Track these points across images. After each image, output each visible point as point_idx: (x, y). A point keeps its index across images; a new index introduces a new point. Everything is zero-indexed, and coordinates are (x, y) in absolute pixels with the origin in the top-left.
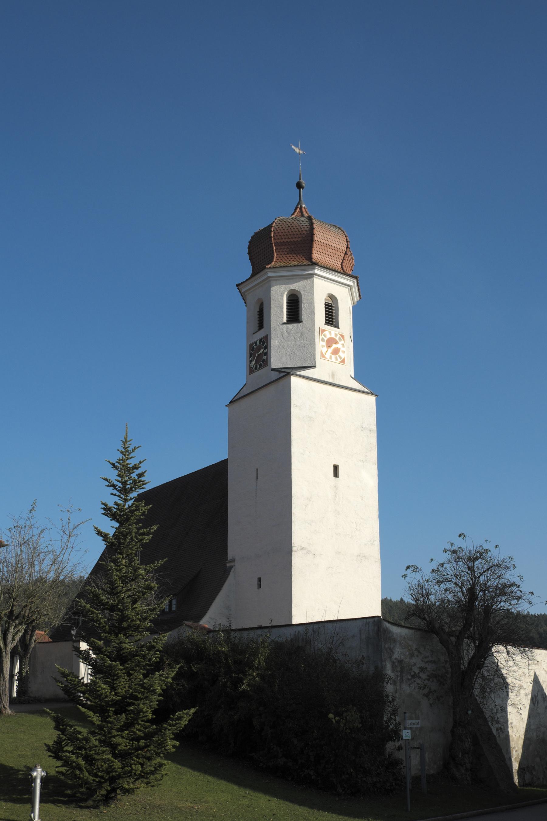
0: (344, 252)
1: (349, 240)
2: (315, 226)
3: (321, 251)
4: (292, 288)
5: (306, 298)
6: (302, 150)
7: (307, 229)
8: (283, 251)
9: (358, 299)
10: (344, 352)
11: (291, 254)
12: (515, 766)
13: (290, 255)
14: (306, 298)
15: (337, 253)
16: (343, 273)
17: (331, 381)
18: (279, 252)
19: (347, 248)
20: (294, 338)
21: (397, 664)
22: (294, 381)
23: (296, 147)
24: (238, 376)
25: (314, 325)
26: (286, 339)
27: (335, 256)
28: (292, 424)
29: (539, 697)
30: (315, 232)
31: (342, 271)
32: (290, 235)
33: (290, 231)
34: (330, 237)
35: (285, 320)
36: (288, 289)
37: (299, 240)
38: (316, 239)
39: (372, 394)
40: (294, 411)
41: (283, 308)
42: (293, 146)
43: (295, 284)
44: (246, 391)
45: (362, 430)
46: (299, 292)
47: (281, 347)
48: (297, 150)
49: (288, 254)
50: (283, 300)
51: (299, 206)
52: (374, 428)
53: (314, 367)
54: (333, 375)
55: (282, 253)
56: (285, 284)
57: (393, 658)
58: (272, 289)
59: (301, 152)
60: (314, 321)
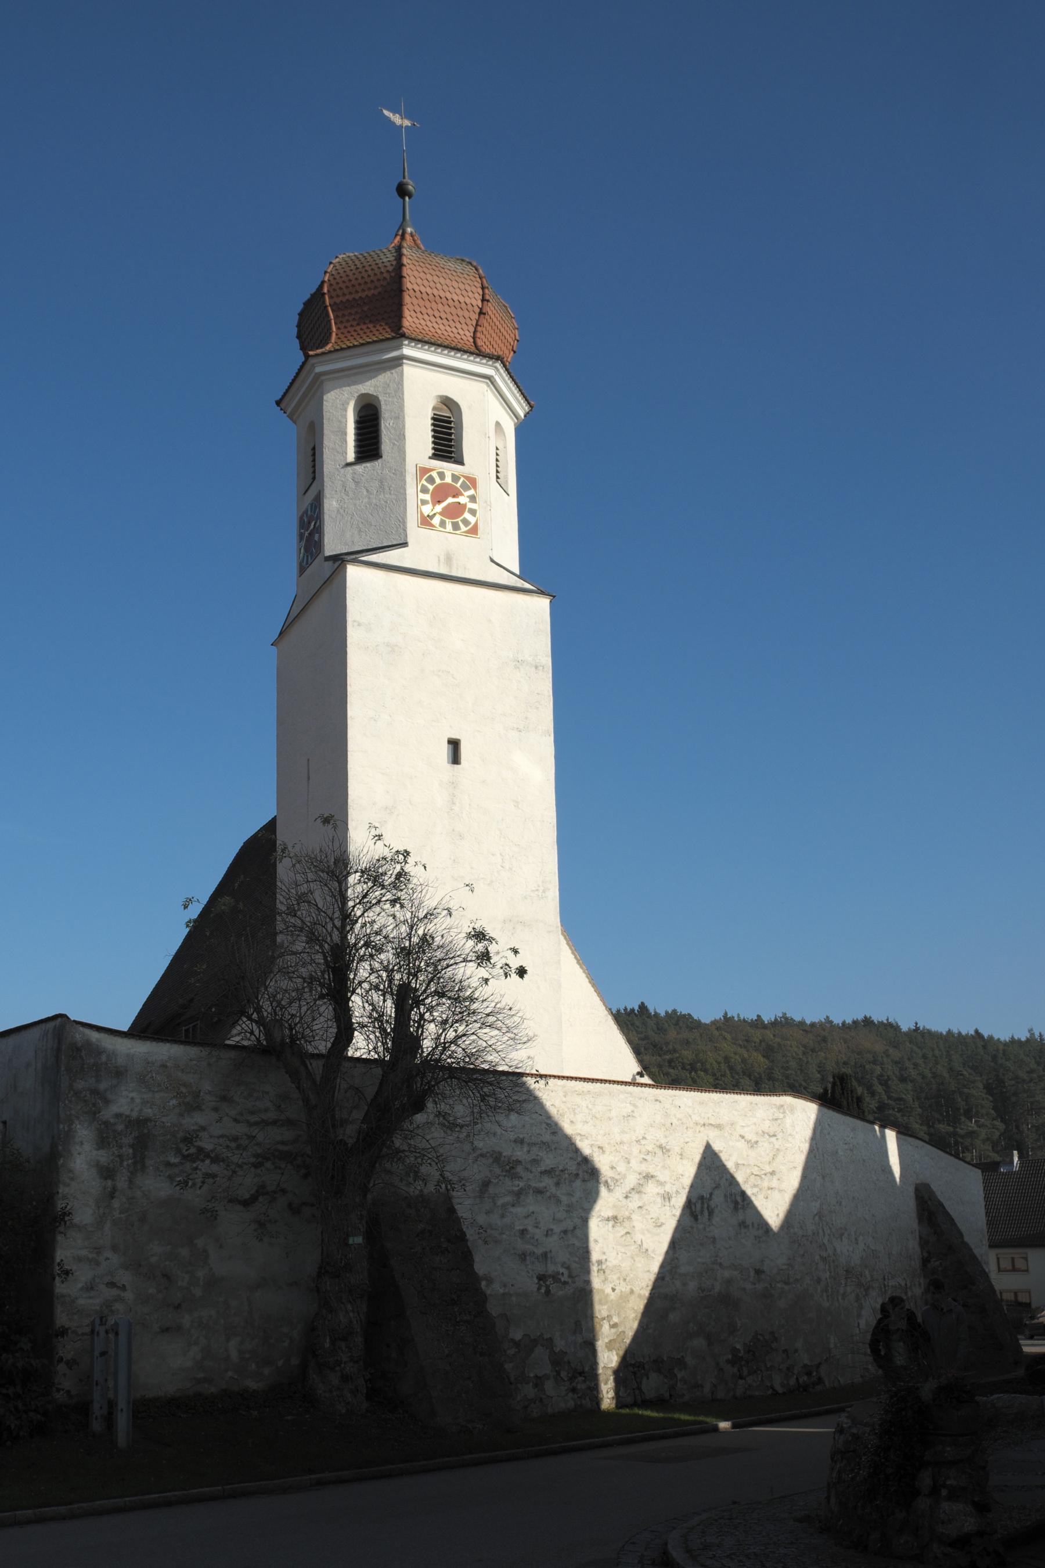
0: (478, 310)
1: (486, 285)
2: (405, 261)
3: (424, 310)
4: (363, 392)
5: (388, 407)
6: (407, 117)
7: (390, 269)
8: (348, 321)
9: (527, 408)
10: (473, 512)
11: (365, 323)
12: (608, 1359)
13: (362, 326)
14: (388, 407)
15: (460, 313)
16: (477, 352)
17: (443, 570)
18: (342, 322)
19: (483, 300)
20: (367, 491)
21: (120, 1127)
22: (353, 573)
23: (394, 112)
24: (284, 586)
25: (404, 460)
26: (351, 494)
27: (456, 319)
28: (349, 661)
29: (718, 1199)
30: (406, 271)
31: (473, 349)
32: (360, 284)
33: (359, 276)
34: (436, 279)
35: (351, 456)
36: (356, 395)
37: (376, 292)
38: (409, 286)
39: (542, 592)
40: (354, 635)
41: (346, 434)
42: (386, 112)
43: (368, 383)
44: (296, 611)
45: (516, 667)
46: (376, 398)
47: (342, 511)
48: (397, 119)
49: (358, 324)
50: (345, 417)
51: (400, 232)
52: (547, 661)
53: (404, 544)
54: (449, 559)
55: (348, 325)
56: (349, 385)
57: (108, 1114)
58: (325, 397)
59: (407, 123)
60: (404, 452)
